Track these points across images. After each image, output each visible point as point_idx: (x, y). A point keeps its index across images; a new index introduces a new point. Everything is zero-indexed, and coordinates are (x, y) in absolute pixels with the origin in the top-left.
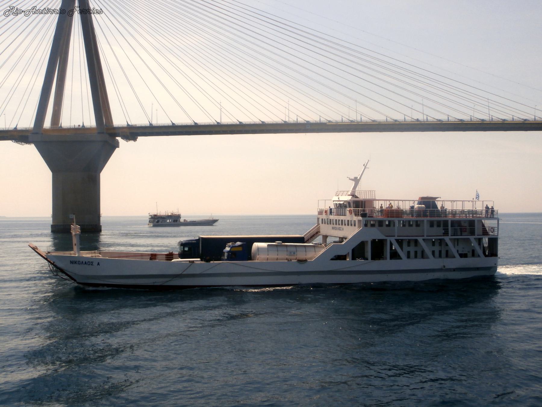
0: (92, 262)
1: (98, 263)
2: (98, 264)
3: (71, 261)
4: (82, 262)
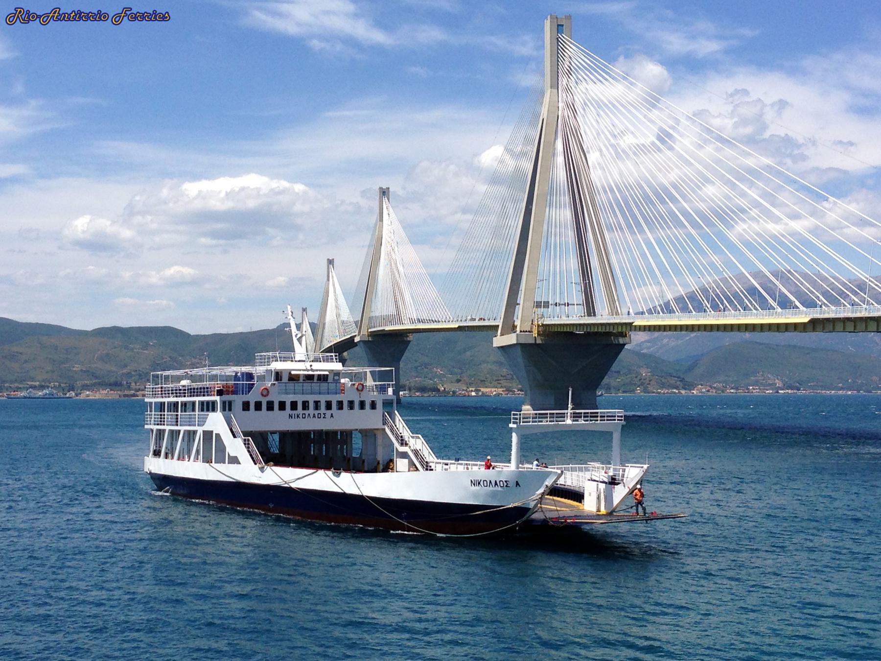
0: (506, 481)
1: (517, 482)
2: (517, 484)
3: (472, 482)
4: (490, 482)
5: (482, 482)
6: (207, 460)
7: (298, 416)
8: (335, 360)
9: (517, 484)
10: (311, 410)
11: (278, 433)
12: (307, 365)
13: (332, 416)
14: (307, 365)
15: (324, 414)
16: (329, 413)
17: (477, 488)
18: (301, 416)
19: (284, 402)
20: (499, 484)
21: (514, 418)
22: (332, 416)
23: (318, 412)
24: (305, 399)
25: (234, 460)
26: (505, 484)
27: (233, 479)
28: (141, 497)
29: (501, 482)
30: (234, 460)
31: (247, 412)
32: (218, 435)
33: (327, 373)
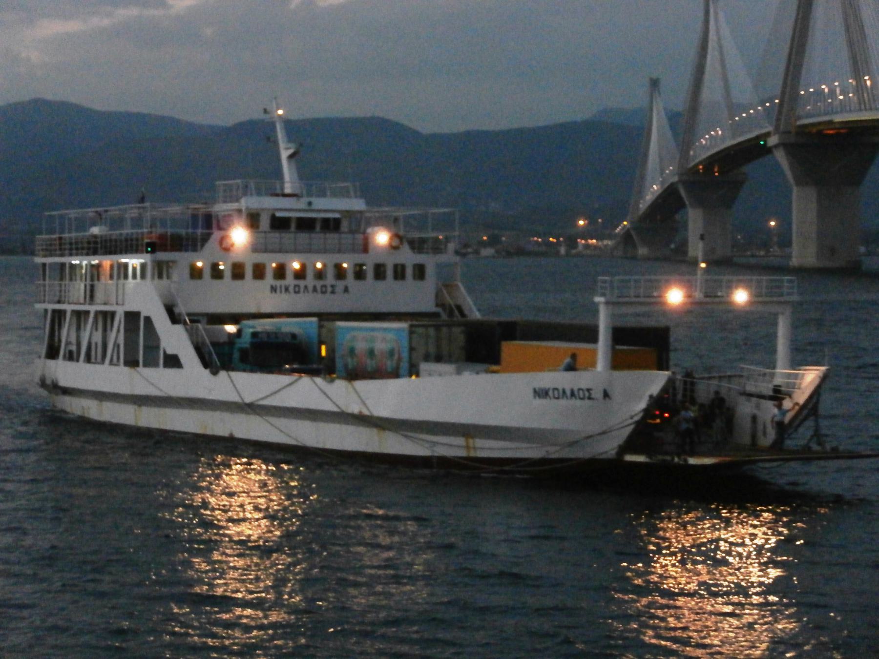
2: (606, 395)
5: (561, 396)
6: (132, 363)
7: (287, 289)
8: (352, 193)
9: (606, 395)
10: (269, 279)
11: (322, 323)
12: (302, 204)
13: (346, 290)
14: (302, 204)
15: (332, 286)
16: (340, 285)
17: (544, 402)
18: (291, 289)
19: (403, 267)
20: (577, 395)
21: (602, 288)
22: (346, 290)
23: (322, 283)
24: (360, 261)
25: (173, 362)
26: (587, 394)
27: (267, 421)
28: (250, 527)
29: (581, 392)
30: (173, 362)
31: (199, 282)
32: (148, 320)
33: (337, 216)
